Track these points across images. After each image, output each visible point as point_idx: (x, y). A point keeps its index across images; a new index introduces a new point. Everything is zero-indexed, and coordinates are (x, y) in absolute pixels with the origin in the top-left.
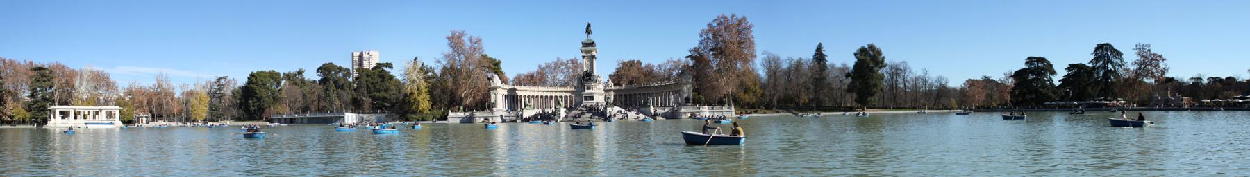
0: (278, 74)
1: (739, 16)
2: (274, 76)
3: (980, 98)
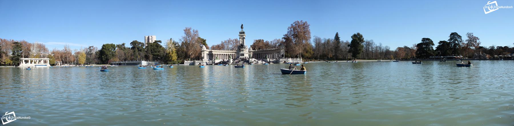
0: (114, 45)
1: (304, 21)
2: (113, 46)
3: (403, 55)
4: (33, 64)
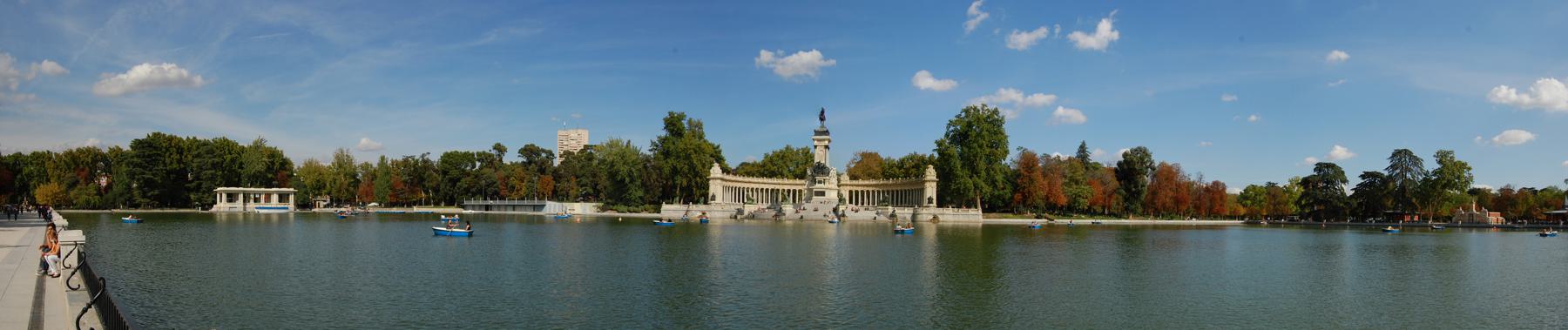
1: (991, 108)
2: (468, 157)
3: (1264, 207)
4: (251, 206)
